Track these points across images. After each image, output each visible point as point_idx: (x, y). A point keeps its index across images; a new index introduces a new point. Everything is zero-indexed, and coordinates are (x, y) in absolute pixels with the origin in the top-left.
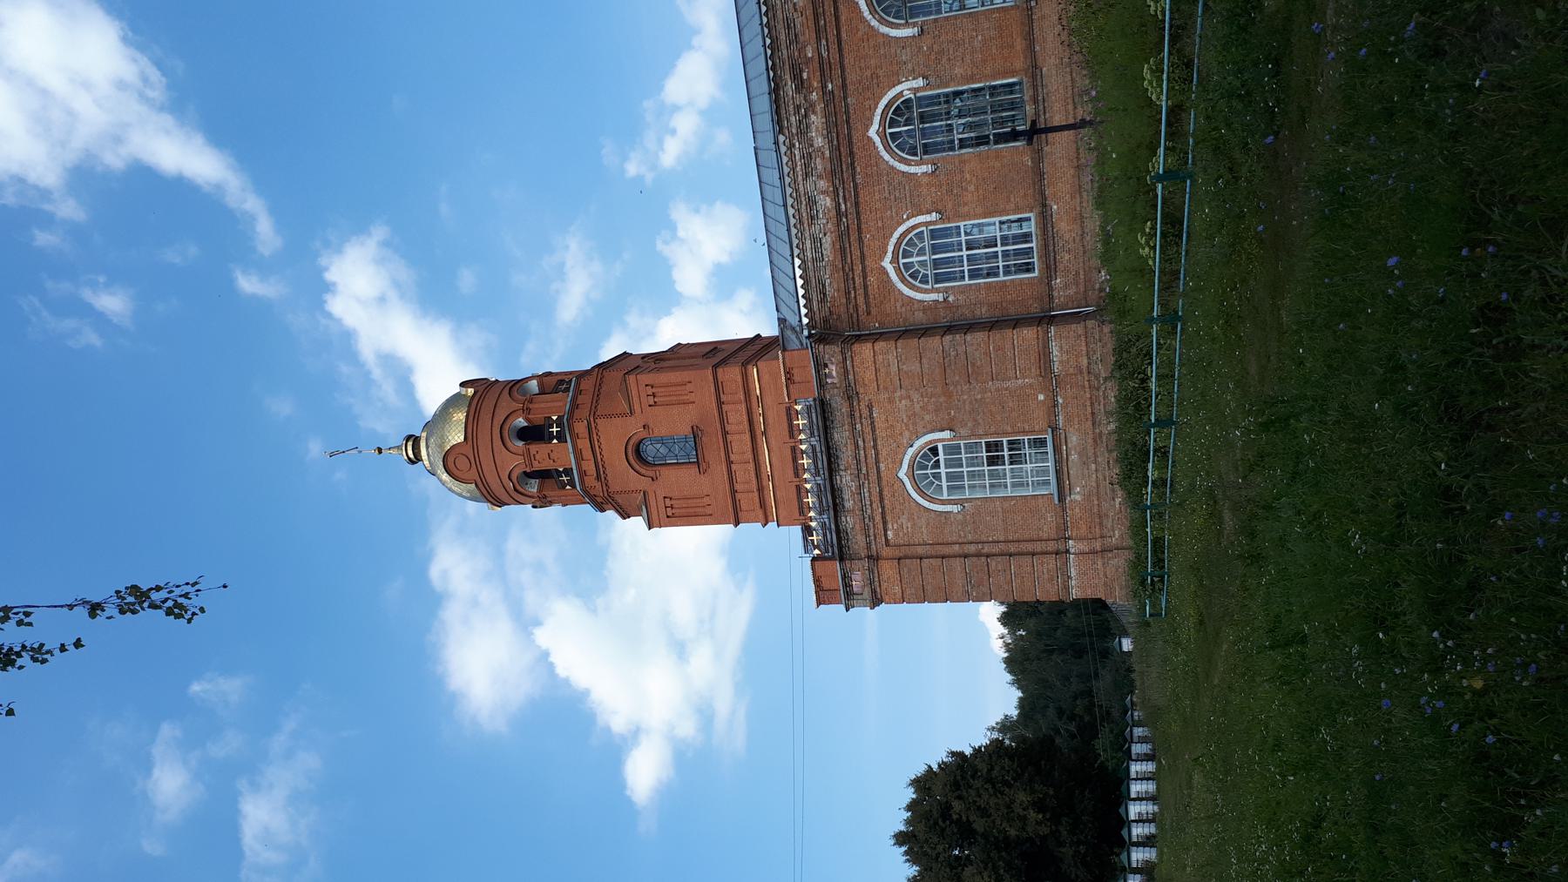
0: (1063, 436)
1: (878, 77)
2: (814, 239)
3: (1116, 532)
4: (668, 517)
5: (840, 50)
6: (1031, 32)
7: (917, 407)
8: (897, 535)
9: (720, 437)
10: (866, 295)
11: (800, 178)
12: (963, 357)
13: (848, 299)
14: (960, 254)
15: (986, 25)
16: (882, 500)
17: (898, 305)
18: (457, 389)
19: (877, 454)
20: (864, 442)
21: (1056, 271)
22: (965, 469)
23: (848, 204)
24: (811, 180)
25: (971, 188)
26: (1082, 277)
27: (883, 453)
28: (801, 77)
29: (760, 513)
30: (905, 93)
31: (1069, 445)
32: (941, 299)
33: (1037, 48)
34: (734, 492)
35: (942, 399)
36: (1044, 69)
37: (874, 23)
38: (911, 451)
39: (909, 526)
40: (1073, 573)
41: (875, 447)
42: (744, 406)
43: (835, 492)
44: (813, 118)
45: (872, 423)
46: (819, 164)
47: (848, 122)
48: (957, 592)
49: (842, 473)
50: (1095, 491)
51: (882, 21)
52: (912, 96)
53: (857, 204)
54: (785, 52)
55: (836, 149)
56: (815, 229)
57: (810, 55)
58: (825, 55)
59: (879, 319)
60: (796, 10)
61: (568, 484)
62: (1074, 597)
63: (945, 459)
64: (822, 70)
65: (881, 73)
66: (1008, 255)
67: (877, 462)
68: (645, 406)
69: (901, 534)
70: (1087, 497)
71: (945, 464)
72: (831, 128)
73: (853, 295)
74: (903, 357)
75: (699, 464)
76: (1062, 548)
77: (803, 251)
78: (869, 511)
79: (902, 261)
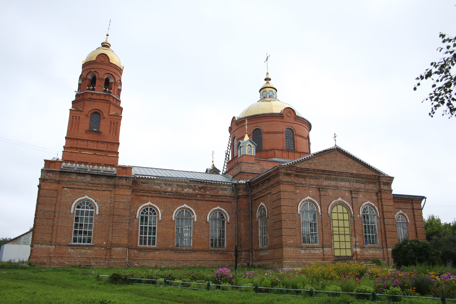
0: (91, 248)
1: (198, 209)
2: (160, 184)
3: (56, 261)
4: (73, 116)
5: (207, 201)
6: (203, 251)
7: (108, 205)
8: (65, 191)
9: (97, 140)
10: (141, 196)
11: (177, 183)
12: (122, 222)
13: (141, 190)
14: (148, 225)
15: (206, 239)
16: (79, 189)
17: (137, 204)
19: (94, 190)
20: (99, 187)
21: (139, 251)
22: (84, 217)
23: (168, 195)
24: (176, 186)
25: (166, 230)
26: (136, 258)
27: (94, 192)
28: (202, 189)
29: (69, 146)
30: (193, 216)
31: (87, 250)
32: (136, 217)
33: (199, 252)
34: (77, 139)
35: (109, 213)
36: (193, 253)
37: (212, 210)
38: (94, 201)
39: (68, 196)
40: (43, 246)
41: (97, 190)
42: (105, 150)
43: (85, 174)
44: (191, 190)
45: (105, 191)
46: (180, 189)
47: (189, 199)
48: (42, 207)
49: (90, 178)
50: (71, 256)
51: (212, 212)
52: (192, 218)
53: (167, 198)
54: (209, 186)
55: (182, 195)
56: (163, 185)
57: (207, 192)
58: (206, 196)
59: (134, 198)
60: (218, 191)
61: (89, 88)
62: (34, 246)
63: (89, 211)
64: (203, 195)
65: (199, 210)
66: (145, 238)
67: (92, 190)
68: (111, 120)
69: (65, 192)
70: (69, 254)
71: (92, 211)
73: (142, 192)
74: (125, 204)
75: (90, 131)
76: (53, 243)
77: (158, 180)
78: (75, 184)
79: (149, 208)
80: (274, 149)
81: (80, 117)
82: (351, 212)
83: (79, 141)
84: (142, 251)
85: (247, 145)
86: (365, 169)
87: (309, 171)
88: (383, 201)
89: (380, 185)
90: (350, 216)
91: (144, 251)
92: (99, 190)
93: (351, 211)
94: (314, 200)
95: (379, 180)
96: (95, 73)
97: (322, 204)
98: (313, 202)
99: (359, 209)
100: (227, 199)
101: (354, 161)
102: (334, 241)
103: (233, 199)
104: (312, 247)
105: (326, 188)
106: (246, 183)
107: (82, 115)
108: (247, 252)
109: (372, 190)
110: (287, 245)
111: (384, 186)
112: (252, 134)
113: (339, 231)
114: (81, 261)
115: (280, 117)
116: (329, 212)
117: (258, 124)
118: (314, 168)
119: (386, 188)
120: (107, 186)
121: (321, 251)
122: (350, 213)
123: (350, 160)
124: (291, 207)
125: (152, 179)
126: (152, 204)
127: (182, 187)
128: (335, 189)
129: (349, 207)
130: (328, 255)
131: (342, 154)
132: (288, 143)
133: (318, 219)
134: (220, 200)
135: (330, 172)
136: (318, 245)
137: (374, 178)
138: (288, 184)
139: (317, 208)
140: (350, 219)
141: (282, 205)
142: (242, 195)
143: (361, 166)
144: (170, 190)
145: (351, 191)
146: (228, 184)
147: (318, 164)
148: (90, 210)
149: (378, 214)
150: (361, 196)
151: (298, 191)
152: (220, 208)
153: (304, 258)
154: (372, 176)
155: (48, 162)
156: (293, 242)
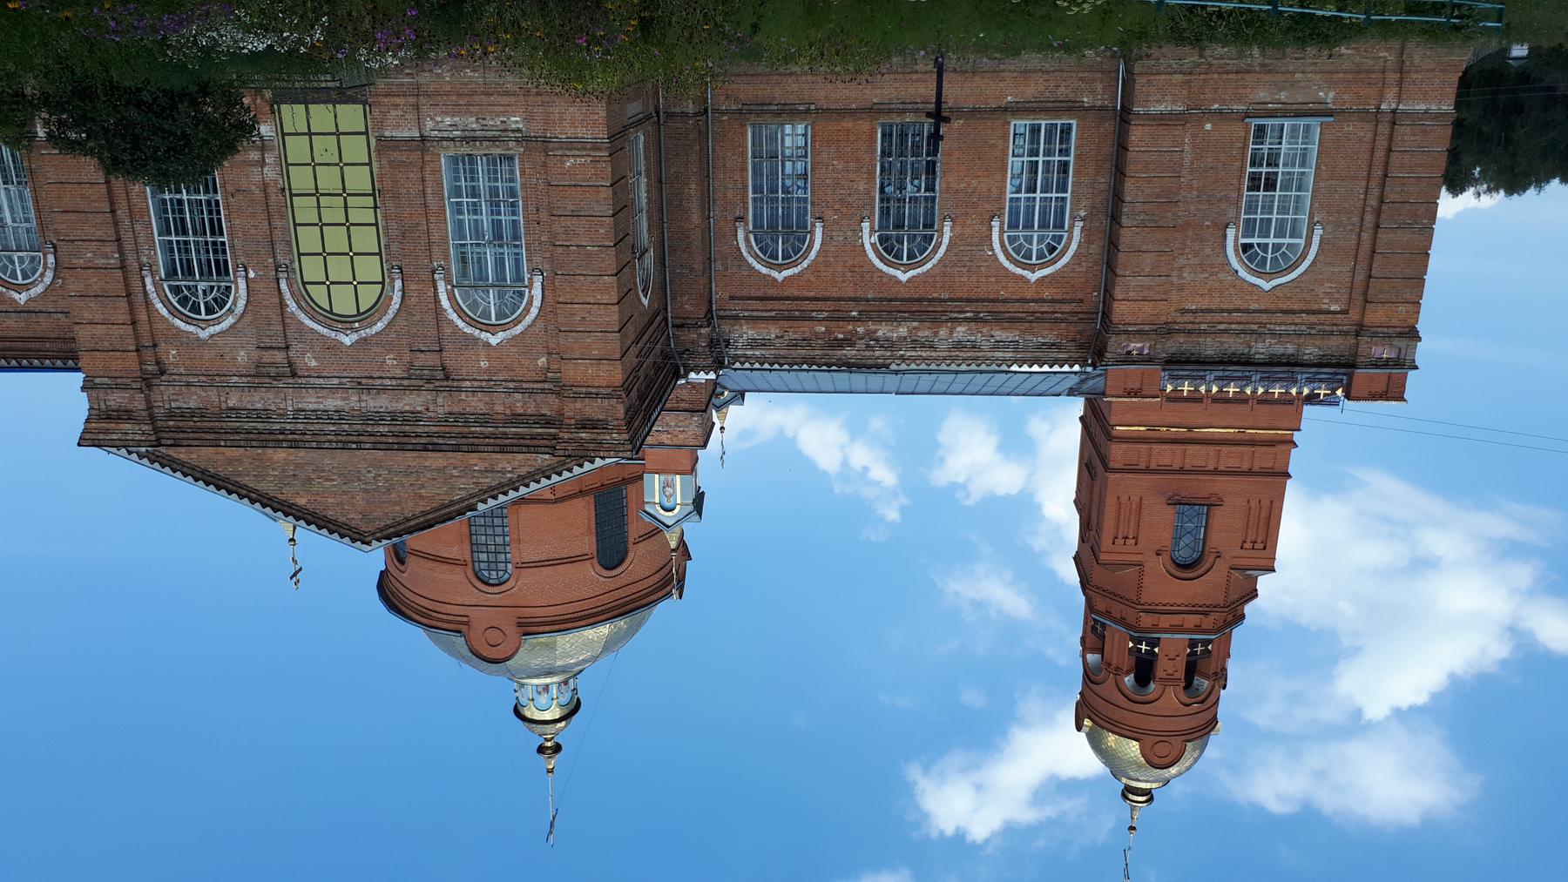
0: (1257, 107)
1: (854, 266)
2: (995, 348)
3: (1381, 55)
7: (1194, 261)
8: (1336, 301)
11: (933, 354)
12: (1147, 206)
13: (1062, 320)
14: (1038, 200)
15: (825, 155)
18: (1082, 736)
19: (1238, 310)
26: (1086, 74)
27: (1238, 303)
30: (873, 240)
31: (1268, 100)
34: (1250, 473)
36: (875, 101)
37: (805, 264)
38: (1243, 273)
39: (1329, 285)
41: (1230, 311)
42: (1154, 446)
43: (1274, 362)
44: (880, 333)
45: (1202, 311)
46: (924, 333)
47: (890, 300)
51: (805, 257)
52: (877, 234)
53: (968, 300)
54: (817, 352)
56: (985, 345)
58: (826, 314)
60: (782, 337)
64: (839, 319)
65: (851, 263)
67: (1247, 311)
68: (1136, 549)
70: (1332, 84)
72: (891, 317)
75: (1211, 504)
77: (1004, 360)
78: (1303, 328)
80: (556, 501)
81: (1242, 548)
82: (290, 286)
83: (1245, 467)
84: (1061, 102)
85: (678, 507)
86: (224, 470)
87: (498, 442)
88: (132, 341)
89: (150, 407)
90: (295, 273)
91: (1057, 104)
92: (1222, 311)
93: (292, 294)
94: (468, 330)
95: (156, 430)
96: (1189, 701)
97: (430, 318)
98: (472, 323)
99: (248, 301)
100: (747, 310)
101: (279, 496)
102: (370, 164)
103: (726, 310)
104: (475, 139)
105: (413, 380)
106: (686, 375)
107: (1235, 554)
108: (677, 110)
109: (189, 385)
110: (592, 149)
111: (130, 407)
112: (630, 545)
113: (319, 207)
114: (1296, 58)
115: (530, 624)
116: (398, 284)
117: (613, 584)
118: (473, 458)
119: (116, 399)
120: (1197, 326)
121: (429, 124)
122: (295, 286)
123: (302, 501)
124: (576, 301)
125: (1015, 362)
126: (1026, 273)
127: (916, 343)
128: (372, 378)
129: (300, 307)
130: (396, 106)
131: (342, 519)
132: (499, 530)
133: (446, 256)
134: (776, 305)
135: (402, 448)
136: (447, 148)
137: (182, 435)
138: (590, 390)
139: (451, 298)
140: (292, 262)
141: (616, 308)
142: (701, 326)
143: (249, 481)
144: (959, 329)
145: (294, 375)
146: (747, 365)
147: (455, 473)
148: (1255, 241)
149: (154, 283)
150: (242, 356)
151: (542, 361)
152: (775, 274)
153: (507, 93)
154: (190, 442)
155: (1394, 394)
156: (564, 162)
